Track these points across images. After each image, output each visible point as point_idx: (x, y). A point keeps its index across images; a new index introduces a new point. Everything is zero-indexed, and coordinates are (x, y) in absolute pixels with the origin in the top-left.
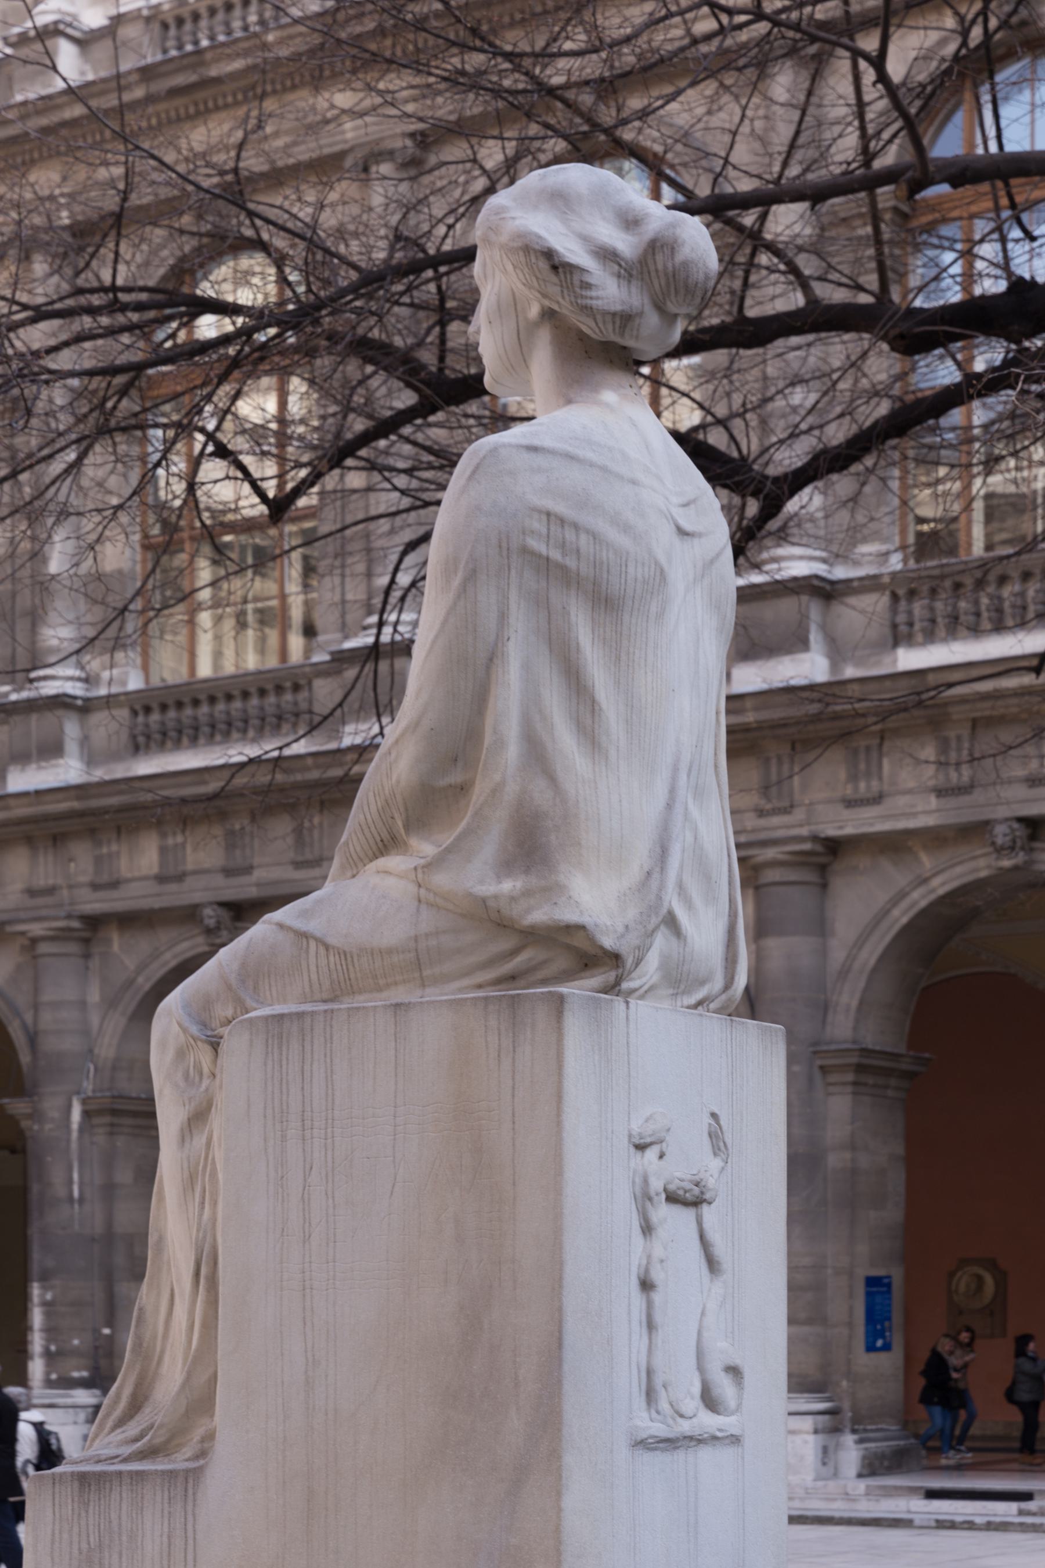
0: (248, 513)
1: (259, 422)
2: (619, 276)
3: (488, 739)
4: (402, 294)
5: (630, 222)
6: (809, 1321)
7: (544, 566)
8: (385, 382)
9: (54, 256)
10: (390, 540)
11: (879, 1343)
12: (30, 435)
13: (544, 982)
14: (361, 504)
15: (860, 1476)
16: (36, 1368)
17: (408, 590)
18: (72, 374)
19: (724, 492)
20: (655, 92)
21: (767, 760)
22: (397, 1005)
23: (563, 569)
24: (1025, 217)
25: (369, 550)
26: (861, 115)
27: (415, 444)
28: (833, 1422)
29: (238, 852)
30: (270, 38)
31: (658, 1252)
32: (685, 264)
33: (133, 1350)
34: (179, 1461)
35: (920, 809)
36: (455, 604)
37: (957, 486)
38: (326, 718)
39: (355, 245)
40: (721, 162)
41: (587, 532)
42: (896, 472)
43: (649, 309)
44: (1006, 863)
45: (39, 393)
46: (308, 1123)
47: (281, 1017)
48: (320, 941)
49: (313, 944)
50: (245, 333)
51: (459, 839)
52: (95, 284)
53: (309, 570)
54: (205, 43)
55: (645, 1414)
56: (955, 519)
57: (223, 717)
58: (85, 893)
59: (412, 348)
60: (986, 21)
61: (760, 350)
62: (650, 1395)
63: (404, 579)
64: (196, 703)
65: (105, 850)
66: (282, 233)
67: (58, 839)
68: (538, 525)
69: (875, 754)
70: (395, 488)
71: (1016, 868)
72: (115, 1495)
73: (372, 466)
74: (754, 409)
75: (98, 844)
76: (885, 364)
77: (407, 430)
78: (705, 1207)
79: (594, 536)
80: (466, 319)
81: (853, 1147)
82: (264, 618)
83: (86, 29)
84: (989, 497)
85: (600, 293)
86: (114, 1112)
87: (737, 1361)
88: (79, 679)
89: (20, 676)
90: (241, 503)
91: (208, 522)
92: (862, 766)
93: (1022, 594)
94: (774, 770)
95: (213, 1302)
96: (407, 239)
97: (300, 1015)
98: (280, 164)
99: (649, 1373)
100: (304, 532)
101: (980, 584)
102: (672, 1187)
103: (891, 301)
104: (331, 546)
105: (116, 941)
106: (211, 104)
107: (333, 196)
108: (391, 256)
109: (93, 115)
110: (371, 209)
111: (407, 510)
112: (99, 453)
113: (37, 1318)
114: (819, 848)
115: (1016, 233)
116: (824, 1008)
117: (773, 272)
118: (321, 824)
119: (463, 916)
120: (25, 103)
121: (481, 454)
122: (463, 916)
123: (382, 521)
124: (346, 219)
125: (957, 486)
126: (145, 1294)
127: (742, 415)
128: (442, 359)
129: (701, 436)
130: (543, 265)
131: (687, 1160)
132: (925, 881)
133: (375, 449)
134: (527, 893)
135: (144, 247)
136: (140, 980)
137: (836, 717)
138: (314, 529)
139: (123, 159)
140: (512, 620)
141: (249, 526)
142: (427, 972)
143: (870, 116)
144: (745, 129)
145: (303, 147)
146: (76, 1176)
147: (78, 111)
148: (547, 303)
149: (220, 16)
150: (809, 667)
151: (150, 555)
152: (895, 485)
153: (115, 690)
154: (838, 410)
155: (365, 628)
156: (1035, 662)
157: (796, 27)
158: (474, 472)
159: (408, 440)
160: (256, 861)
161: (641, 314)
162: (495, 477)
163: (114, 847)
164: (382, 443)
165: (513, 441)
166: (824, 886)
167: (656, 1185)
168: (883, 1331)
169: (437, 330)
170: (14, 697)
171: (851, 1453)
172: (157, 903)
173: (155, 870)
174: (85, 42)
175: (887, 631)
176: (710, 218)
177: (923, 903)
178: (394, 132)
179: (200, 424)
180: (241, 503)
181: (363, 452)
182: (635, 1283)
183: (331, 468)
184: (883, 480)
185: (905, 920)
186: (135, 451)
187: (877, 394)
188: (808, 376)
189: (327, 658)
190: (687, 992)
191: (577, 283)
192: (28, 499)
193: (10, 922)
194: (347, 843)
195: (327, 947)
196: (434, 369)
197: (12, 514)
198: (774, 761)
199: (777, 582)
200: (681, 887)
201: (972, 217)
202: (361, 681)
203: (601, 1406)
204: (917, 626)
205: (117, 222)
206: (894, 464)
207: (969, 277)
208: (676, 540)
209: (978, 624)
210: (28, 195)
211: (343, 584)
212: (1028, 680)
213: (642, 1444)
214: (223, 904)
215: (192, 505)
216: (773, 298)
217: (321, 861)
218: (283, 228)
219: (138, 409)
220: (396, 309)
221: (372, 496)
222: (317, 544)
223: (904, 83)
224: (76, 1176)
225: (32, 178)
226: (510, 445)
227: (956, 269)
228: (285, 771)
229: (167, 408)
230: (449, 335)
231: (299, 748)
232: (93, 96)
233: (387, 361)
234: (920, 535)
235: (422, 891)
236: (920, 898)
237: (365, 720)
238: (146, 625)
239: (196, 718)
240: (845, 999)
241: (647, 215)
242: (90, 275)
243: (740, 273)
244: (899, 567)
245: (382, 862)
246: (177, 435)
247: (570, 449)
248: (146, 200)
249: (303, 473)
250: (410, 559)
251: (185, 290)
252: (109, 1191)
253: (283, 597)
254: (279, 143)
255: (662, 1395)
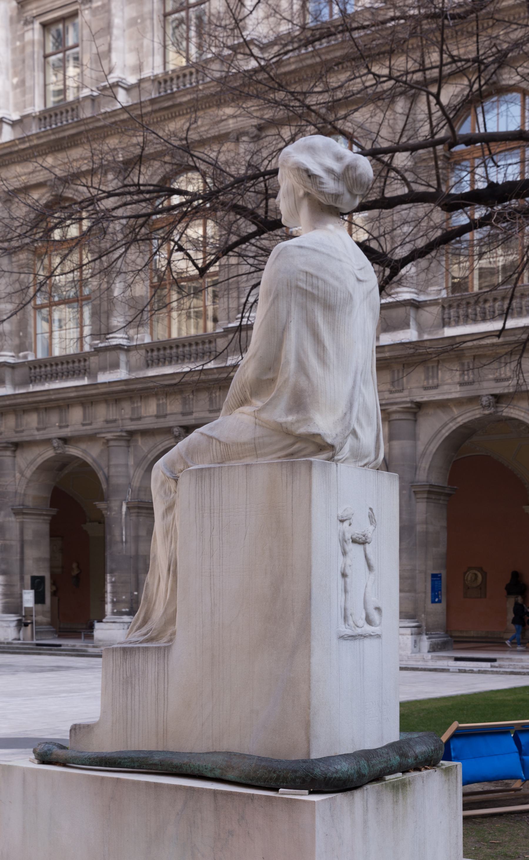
0: (192, 273)
1: (195, 237)
2: (334, 179)
3: (283, 361)
4: (250, 187)
5: (339, 158)
6: (409, 591)
7: (305, 293)
8: (244, 222)
9: (116, 172)
10: (246, 284)
11: (437, 600)
12: (106, 242)
13: (304, 456)
14: (236, 270)
15: (429, 652)
16: (108, 608)
17: (253, 304)
18: (122, 218)
19: (377, 266)
20: (350, 109)
21: (393, 371)
22: (247, 465)
23: (312, 294)
24: (495, 158)
25: (238, 288)
26: (430, 118)
27: (256, 246)
28: (418, 631)
29: (187, 406)
30: (201, 87)
31: (349, 562)
32: (360, 175)
33: (144, 600)
34: (162, 643)
35: (453, 391)
36: (270, 308)
37: (468, 264)
38: (221, 353)
39: (233, 168)
40: (375, 135)
41: (322, 280)
42: (444, 258)
43: (346, 192)
44: (487, 412)
45: (109, 225)
46: (212, 511)
47: (202, 469)
48: (217, 440)
49: (214, 441)
50: (189, 202)
51: (271, 400)
52: (132, 183)
53: (215, 296)
54: (175, 90)
55: (343, 626)
56: (467, 277)
57: (182, 353)
58: (128, 422)
59: (254, 209)
60: (480, 81)
61: (391, 210)
62: (345, 618)
63: (251, 299)
64: (171, 348)
65: (135, 405)
66: (204, 163)
67: (117, 401)
68: (302, 277)
69: (435, 369)
70: (248, 264)
71: (490, 414)
72: (137, 656)
73: (239, 255)
74: (388, 233)
75: (133, 403)
76: (440, 215)
77: (253, 241)
78: (367, 545)
79: (325, 281)
80: (275, 197)
81: (426, 523)
82: (198, 315)
83: (129, 84)
84: (480, 269)
85: (327, 186)
86: (139, 508)
87: (380, 605)
88: (126, 339)
89: (103, 336)
90: (189, 269)
91: (176, 277)
92: (431, 374)
93: (493, 307)
94: (396, 375)
95: (175, 581)
96: (253, 166)
97: (209, 469)
98: (205, 137)
99: (345, 609)
100: (213, 281)
101: (477, 302)
102: (354, 537)
103: (442, 191)
104: (223, 286)
105: (140, 441)
106: (177, 114)
107: (224, 148)
108: (246, 172)
109: (132, 118)
110: (239, 154)
111: (253, 272)
112: (133, 249)
113: (109, 588)
114: (414, 406)
115: (491, 164)
116: (415, 469)
117: (395, 179)
118: (220, 396)
119: (273, 430)
120: (105, 113)
121: (281, 249)
122: (273, 430)
123: (244, 276)
124: (229, 158)
125: (468, 264)
126: (149, 578)
127: (384, 236)
128: (266, 212)
129: (368, 244)
130: (305, 175)
131: (360, 526)
132: (455, 419)
133: (241, 248)
134: (298, 421)
135: (151, 169)
136: (149, 456)
137: (420, 354)
138: (217, 280)
139: (142, 134)
140: (292, 314)
141: (191, 279)
142: (259, 452)
143: (433, 118)
144: (386, 123)
145: (213, 131)
146: (124, 533)
147: (125, 116)
148: (306, 190)
149: (181, 79)
150: (410, 335)
151: (153, 290)
152: (443, 263)
153: (139, 343)
154: (421, 234)
155: (237, 319)
156: (498, 333)
157: (405, 82)
158: (277, 256)
159: (253, 245)
160: (194, 410)
161: (343, 194)
162: (285, 258)
163: (139, 404)
164: (244, 246)
165: (293, 244)
166: (416, 421)
167: (348, 536)
168: (438, 595)
169: (264, 202)
170: (100, 345)
171: (425, 643)
172: (156, 426)
173: (155, 413)
174: (128, 89)
175: (441, 321)
176: (371, 158)
177: (454, 428)
178: (249, 123)
179: (172, 238)
180: (189, 269)
181: (236, 250)
182: (339, 575)
183: (223, 256)
184: (439, 261)
185: (447, 434)
186: (148, 249)
187: (436, 227)
188: (410, 220)
189: (222, 330)
190: (360, 460)
191: (318, 182)
192: (105, 267)
193: (99, 433)
194: (228, 401)
195: (220, 442)
196: (263, 217)
197: (99, 273)
198: (396, 372)
199: (397, 301)
200: (358, 419)
201: (474, 158)
202: (235, 339)
203: (327, 623)
204: (452, 319)
205: (140, 160)
206: (443, 255)
207: (473, 181)
208: (356, 283)
209: (476, 318)
210: (106, 148)
211: (228, 300)
212: (495, 340)
213: (342, 638)
214: (181, 427)
215: (169, 269)
216: (397, 189)
217: (219, 410)
218: (204, 161)
219: (148, 232)
220: (249, 193)
221: (239, 266)
222: (218, 285)
223: (448, 105)
224: (124, 533)
225: (107, 142)
226: (292, 246)
227: (468, 178)
228: (205, 375)
229: (160, 232)
230: (269, 204)
231: (211, 365)
232: (131, 110)
233: (245, 213)
234: (453, 284)
235: (257, 420)
236: (453, 426)
237: (236, 355)
238: (151, 316)
239: (171, 354)
240: (423, 465)
241: (345, 155)
242: (130, 180)
243: (383, 180)
244: (445, 296)
245: (241, 409)
246: (163, 242)
247: (315, 247)
248: (152, 151)
249: (213, 257)
250: (254, 292)
251: (167, 186)
252: (137, 538)
253: (205, 307)
254: (203, 129)
255: (350, 618)
